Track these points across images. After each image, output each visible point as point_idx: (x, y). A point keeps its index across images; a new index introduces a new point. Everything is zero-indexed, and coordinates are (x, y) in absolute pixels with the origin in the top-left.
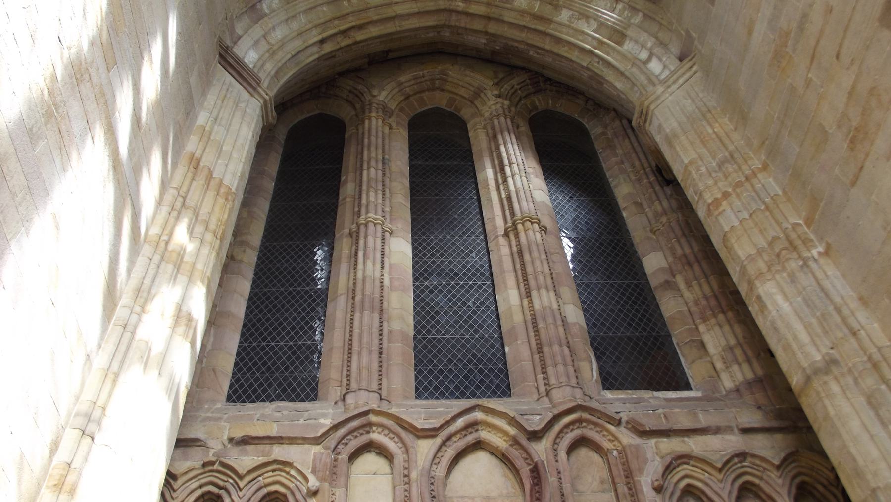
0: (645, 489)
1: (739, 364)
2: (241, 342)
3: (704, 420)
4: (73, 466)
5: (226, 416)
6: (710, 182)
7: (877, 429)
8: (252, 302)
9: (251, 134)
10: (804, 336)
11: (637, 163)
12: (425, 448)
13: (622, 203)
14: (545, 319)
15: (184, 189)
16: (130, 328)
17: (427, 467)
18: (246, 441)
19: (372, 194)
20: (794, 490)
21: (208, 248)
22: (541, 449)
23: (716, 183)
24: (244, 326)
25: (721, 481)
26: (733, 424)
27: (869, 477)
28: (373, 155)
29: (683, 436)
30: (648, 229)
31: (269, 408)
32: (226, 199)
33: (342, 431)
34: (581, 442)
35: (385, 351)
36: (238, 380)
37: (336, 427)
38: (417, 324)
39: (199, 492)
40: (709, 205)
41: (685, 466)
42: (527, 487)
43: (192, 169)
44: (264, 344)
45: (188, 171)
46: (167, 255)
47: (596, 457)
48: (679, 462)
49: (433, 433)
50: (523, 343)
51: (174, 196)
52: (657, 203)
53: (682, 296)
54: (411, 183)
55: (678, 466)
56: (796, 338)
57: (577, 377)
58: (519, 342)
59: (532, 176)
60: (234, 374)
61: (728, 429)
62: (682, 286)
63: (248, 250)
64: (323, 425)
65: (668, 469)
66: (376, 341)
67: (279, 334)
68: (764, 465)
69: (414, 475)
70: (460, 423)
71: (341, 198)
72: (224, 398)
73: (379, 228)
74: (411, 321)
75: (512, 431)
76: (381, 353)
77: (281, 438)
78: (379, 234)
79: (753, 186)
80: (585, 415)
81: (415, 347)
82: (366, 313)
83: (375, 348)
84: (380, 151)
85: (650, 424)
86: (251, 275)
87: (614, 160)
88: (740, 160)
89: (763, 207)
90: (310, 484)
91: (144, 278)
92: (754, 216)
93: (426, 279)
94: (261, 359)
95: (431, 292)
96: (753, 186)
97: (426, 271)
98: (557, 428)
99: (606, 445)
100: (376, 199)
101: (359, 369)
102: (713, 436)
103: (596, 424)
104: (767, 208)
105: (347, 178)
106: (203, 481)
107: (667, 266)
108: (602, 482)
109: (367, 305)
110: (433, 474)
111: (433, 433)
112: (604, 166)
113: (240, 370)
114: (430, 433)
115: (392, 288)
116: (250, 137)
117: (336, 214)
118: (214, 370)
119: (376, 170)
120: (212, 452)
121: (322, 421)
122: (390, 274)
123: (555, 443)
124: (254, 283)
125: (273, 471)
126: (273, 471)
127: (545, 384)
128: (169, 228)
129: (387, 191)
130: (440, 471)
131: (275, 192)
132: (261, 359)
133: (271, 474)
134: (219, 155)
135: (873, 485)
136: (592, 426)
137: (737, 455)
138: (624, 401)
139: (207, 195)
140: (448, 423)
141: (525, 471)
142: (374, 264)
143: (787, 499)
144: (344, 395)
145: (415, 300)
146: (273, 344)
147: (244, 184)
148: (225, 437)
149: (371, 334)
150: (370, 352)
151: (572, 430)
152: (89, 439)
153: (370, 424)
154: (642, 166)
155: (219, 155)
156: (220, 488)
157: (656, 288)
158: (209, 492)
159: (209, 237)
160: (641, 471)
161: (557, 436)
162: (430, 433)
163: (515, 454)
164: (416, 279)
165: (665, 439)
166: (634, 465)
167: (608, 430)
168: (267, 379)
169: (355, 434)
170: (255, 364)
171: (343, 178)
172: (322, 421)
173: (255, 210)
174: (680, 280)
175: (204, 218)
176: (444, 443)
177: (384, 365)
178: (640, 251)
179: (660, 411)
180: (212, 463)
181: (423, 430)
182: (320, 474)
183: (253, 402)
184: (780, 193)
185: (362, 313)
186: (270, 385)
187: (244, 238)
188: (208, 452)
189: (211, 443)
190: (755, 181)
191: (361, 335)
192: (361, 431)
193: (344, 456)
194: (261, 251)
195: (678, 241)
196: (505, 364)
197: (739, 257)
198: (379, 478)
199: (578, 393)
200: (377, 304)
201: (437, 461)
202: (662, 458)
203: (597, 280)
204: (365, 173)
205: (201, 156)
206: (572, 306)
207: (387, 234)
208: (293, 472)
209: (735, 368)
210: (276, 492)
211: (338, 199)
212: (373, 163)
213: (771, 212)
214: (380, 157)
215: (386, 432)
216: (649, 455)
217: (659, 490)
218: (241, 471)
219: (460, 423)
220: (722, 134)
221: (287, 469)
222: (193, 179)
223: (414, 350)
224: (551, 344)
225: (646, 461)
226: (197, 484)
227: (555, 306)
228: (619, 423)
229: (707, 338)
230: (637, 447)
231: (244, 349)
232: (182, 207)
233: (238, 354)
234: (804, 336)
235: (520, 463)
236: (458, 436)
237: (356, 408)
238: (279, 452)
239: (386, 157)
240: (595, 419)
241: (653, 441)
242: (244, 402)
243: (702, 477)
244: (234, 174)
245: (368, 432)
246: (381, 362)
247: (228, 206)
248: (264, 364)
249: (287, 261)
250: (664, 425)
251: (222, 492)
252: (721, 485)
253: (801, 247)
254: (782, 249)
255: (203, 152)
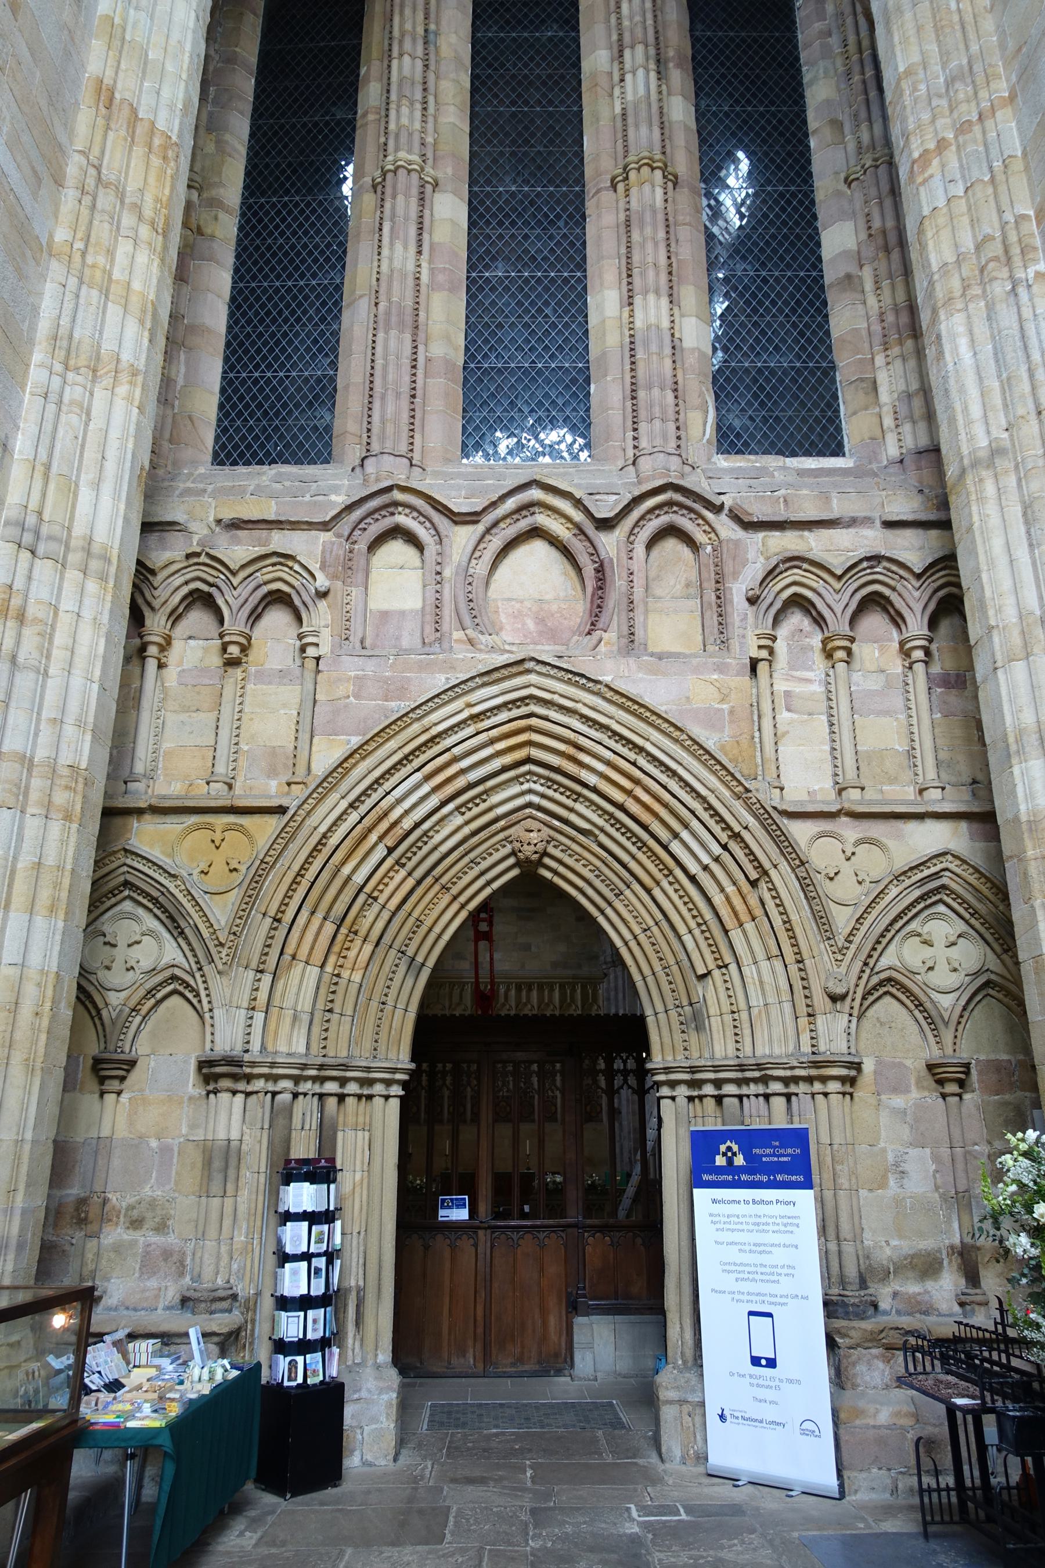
0: (735, 600)
1: (914, 422)
2: (224, 372)
3: (837, 508)
4: (15, 588)
5: (210, 488)
6: (926, 116)
7: (1022, 554)
8: (237, 303)
9: (193, 15)
10: (976, 410)
11: (852, 39)
12: (463, 537)
13: (813, 121)
14: (646, 344)
15: (96, 151)
16: (53, 397)
17: (465, 564)
18: (236, 525)
19: (405, 110)
20: (932, 606)
21: (147, 252)
22: (609, 543)
23: (933, 121)
24: (228, 344)
25: (838, 592)
26: (876, 515)
27: (991, 613)
28: (408, 26)
29: (803, 530)
30: (843, 176)
31: (268, 474)
32: (165, 158)
33: (358, 513)
34: (671, 531)
35: (419, 393)
36: (225, 430)
37: (350, 508)
38: (469, 343)
39: (185, 590)
40: (914, 162)
41: (796, 571)
42: (589, 590)
43: (103, 110)
44: (257, 374)
45: (97, 116)
46: (87, 272)
47: (686, 551)
48: (788, 565)
49: (474, 518)
50: (613, 380)
51: (81, 168)
52: (864, 126)
53: (865, 303)
54: (474, 77)
55: (786, 570)
56: (966, 409)
57: (679, 438)
58: (608, 378)
59: (671, 65)
60: (219, 420)
61: (867, 521)
62: (869, 285)
63: (222, 216)
64: (333, 504)
65: (771, 574)
66: (407, 379)
67: (276, 358)
68: (902, 572)
69: (447, 573)
70: (511, 504)
71: (360, 112)
72: (209, 458)
73: (415, 176)
74: (461, 342)
75: (578, 516)
76: (413, 396)
77: (281, 522)
78: (415, 191)
79: (984, 133)
80: (678, 497)
81: (466, 380)
82: (393, 333)
83: (405, 389)
84: (420, 16)
85: (759, 511)
86: (230, 259)
87: (818, 26)
88: (980, 79)
89: (987, 178)
90: (318, 584)
91: (59, 317)
92: (970, 192)
93: (487, 267)
94: (254, 398)
95: (493, 289)
96: (984, 133)
97: (488, 252)
98: (636, 514)
99: (700, 537)
100: (411, 119)
101: (383, 422)
102: (844, 531)
103: (691, 510)
104: (993, 179)
105: (369, 69)
106: (188, 576)
107: (855, 248)
108: (687, 586)
109: (394, 319)
110: (471, 571)
111: (474, 518)
112: (800, 37)
113: (227, 415)
114: (471, 518)
115: (433, 286)
116: (191, 24)
117: (353, 141)
118: (190, 418)
119: (413, 58)
120: (195, 539)
121: (333, 498)
122: (430, 262)
123: (631, 533)
124: (239, 274)
125: (274, 565)
126: (274, 565)
127: (635, 447)
128: (84, 228)
129: (431, 99)
130: (481, 568)
131: (257, 97)
132: (254, 398)
133: (270, 568)
134: (144, 72)
135: (993, 623)
136: (685, 512)
137: (868, 559)
138: (737, 474)
139: (134, 154)
140: (494, 505)
141: (589, 570)
142: (406, 248)
143: (919, 616)
144: (363, 460)
145: (468, 304)
146: (269, 374)
147: (192, 120)
148: (211, 519)
149: (398, 366)
150: (398, 395)
151: (658, 516)
152: (29, 554)
153: (396, 504)
154: (859, 43)
155: (144, 72)
156: (211, 585)
157: (831, 285)
158: (197, 590)
159: (145, 231)
160: (736, 575)
161: (636, 525)
162: (471, 518)
163: (578, 547)
164: (471, 267)
165: (777, 534)
166: (728, 568)
167: (704, 519)
168: (265, 429)
169: (376, 516)
170: (247, 406)
171: (363, 71)
172: (333, 498)
173: (227, 137)
174: (867, 275)
175: (134, 200)
176: (488, 531)
177: (418, 415)
178: (822, 212)
179: (783, 492)
180: (197, 555)
181: (459, 514)
182: (331, 570)
183: (248, 463)
184: (1019, 154)
185: (386, 333)
186: (269, 438)
187: (214, 193)
188: (191, 538)
189: (193, 526)
190: (989, 124)
191: (385, 367)
192: (383, 513)
193: (362, 546)
194: (243, 215)
195: (881, 204)
196: (588, 410)
197: (930, 265)
198: (407, 573)
199: (675, 463)
200: (409, 319)
201: (477, 554)
202: (767, 559)
203: (745, 270)
204: (395, 63)
205: (115, 82)
206: (694, 320)
207: (429, 188)
208: (297, 567)
209: (907, 428)
210: (278, 591)
211: (356, 113)
212: (408, 45)
213: (995, 188)
214: (420, 30)
215: (415, 514)
216: (751, 555)
217: (752, 601)
218: (233, 566)
219: (511, 504)
220: (969, 18)
221: (290, 564)
222: (108, 128)
223: (464, 385)
224: (649, 388)
225: (745, 563)
226: (182, 580)
227: (665, 324)
228: (718, 509)
229: (883, 378)
230: (737, 543)
231: (230, 383)
232: (97, 187)
233: (223, 391)
234: (976, 410)
235: (584, 559)
236: (508, 521)
237: (377, 480)
238: (279, 541)
239: (432, 27)
240: (688, 502)
241: (761, 535)
242: (234, 463)
243: (814, 585)
244: (171, 107)
245: (392, 514)
246: (413, 410)
247: (169, 172)
248: (260, 406)
249: (282, 234)
250: (781, 514)
251: (213, 590)
252: (837, 597)
253: (1017, 260)
254: (991, 260)
255: (117, 73)
